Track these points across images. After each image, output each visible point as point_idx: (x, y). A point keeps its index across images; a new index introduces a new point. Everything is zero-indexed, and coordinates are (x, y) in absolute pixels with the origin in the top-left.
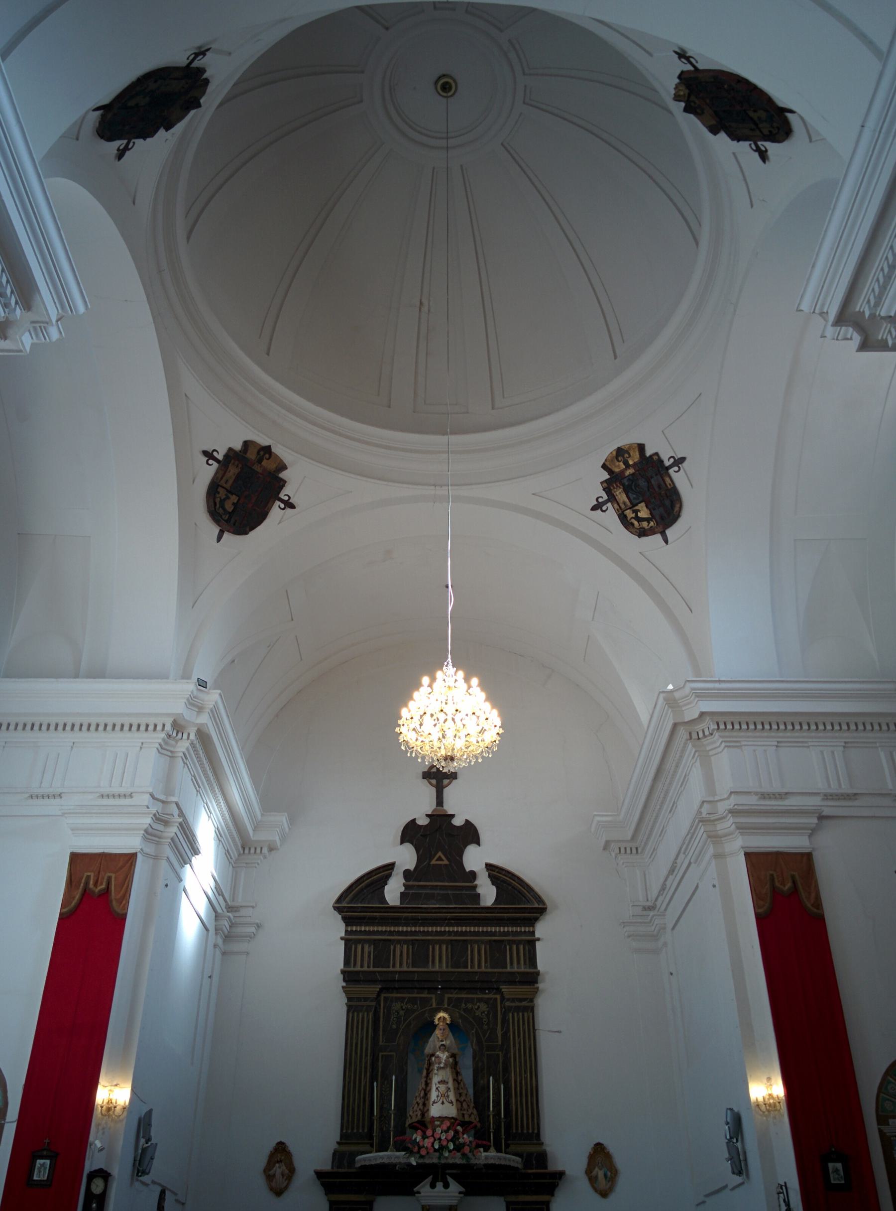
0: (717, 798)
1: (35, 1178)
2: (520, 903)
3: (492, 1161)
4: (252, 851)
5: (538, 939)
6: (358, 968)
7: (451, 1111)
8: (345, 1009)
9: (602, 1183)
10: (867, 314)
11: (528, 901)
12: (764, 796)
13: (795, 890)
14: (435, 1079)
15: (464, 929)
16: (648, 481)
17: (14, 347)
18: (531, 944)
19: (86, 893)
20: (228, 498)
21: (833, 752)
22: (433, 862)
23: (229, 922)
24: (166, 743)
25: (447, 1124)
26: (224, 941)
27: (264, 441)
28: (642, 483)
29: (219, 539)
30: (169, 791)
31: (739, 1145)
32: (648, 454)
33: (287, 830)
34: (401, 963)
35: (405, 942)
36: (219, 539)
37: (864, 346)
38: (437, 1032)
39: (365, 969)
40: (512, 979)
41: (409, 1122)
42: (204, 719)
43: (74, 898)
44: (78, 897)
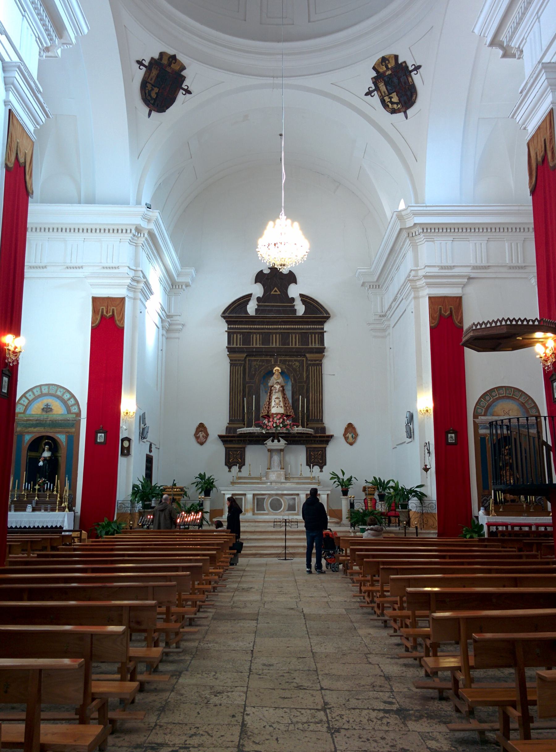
0: (418, 268)
1: (98, 441)
2: (317, 313)
3: (300, 432)
4: (177, 287)
5: (325, 332)
6: (235, 346)
7: (282, 411)
8: (229, 365)
9: (351, 440)
10: (505, 44)
11: (321, 313)
12: (442, 268)
13: (451, 315)
14: (274, 397)
15: (288, 327)
16: (399, 79)
17: (53, 55)
18: (322, 334)
19: (103, 317)
20: (152, 89)
21: (481, 244)
22: (272, 293)
23: (169, 326)
24: (133, 239)
25: (279, 416)
26: (166, 332)
27: (171, 52)
28: (395, 80)
29: (149, 115)
30: (137, 264)
31: (411, 426)
32: (400, 62)
33: (194, 276)
34: (256, 343)
35: (258, 333)
36: (149, 115)
37: (505, 56)
38: (275, 376)
39: (238, 346)
40: (312, 351)
41: (261, 415)
42: (152, 226)
43: (97, 319)
44: (99, 318)
